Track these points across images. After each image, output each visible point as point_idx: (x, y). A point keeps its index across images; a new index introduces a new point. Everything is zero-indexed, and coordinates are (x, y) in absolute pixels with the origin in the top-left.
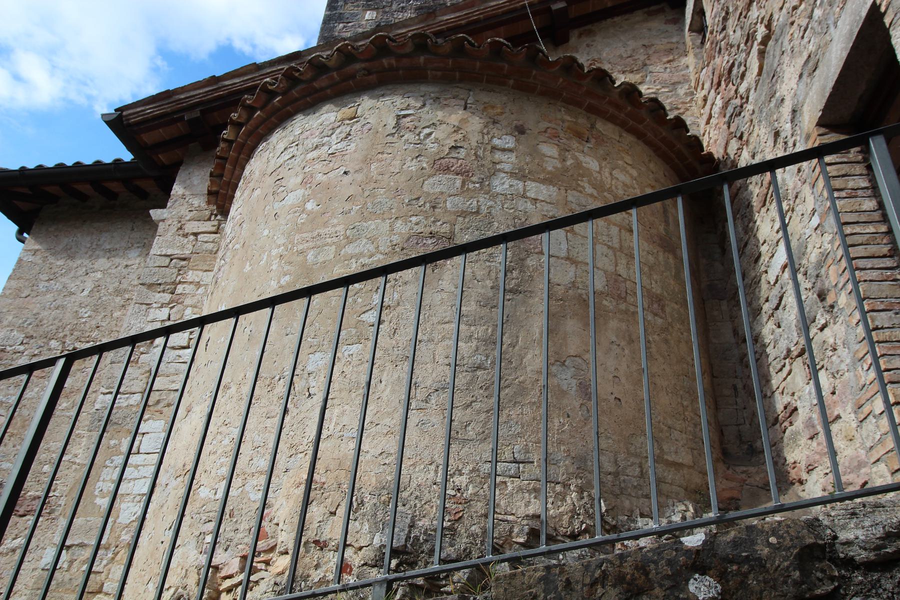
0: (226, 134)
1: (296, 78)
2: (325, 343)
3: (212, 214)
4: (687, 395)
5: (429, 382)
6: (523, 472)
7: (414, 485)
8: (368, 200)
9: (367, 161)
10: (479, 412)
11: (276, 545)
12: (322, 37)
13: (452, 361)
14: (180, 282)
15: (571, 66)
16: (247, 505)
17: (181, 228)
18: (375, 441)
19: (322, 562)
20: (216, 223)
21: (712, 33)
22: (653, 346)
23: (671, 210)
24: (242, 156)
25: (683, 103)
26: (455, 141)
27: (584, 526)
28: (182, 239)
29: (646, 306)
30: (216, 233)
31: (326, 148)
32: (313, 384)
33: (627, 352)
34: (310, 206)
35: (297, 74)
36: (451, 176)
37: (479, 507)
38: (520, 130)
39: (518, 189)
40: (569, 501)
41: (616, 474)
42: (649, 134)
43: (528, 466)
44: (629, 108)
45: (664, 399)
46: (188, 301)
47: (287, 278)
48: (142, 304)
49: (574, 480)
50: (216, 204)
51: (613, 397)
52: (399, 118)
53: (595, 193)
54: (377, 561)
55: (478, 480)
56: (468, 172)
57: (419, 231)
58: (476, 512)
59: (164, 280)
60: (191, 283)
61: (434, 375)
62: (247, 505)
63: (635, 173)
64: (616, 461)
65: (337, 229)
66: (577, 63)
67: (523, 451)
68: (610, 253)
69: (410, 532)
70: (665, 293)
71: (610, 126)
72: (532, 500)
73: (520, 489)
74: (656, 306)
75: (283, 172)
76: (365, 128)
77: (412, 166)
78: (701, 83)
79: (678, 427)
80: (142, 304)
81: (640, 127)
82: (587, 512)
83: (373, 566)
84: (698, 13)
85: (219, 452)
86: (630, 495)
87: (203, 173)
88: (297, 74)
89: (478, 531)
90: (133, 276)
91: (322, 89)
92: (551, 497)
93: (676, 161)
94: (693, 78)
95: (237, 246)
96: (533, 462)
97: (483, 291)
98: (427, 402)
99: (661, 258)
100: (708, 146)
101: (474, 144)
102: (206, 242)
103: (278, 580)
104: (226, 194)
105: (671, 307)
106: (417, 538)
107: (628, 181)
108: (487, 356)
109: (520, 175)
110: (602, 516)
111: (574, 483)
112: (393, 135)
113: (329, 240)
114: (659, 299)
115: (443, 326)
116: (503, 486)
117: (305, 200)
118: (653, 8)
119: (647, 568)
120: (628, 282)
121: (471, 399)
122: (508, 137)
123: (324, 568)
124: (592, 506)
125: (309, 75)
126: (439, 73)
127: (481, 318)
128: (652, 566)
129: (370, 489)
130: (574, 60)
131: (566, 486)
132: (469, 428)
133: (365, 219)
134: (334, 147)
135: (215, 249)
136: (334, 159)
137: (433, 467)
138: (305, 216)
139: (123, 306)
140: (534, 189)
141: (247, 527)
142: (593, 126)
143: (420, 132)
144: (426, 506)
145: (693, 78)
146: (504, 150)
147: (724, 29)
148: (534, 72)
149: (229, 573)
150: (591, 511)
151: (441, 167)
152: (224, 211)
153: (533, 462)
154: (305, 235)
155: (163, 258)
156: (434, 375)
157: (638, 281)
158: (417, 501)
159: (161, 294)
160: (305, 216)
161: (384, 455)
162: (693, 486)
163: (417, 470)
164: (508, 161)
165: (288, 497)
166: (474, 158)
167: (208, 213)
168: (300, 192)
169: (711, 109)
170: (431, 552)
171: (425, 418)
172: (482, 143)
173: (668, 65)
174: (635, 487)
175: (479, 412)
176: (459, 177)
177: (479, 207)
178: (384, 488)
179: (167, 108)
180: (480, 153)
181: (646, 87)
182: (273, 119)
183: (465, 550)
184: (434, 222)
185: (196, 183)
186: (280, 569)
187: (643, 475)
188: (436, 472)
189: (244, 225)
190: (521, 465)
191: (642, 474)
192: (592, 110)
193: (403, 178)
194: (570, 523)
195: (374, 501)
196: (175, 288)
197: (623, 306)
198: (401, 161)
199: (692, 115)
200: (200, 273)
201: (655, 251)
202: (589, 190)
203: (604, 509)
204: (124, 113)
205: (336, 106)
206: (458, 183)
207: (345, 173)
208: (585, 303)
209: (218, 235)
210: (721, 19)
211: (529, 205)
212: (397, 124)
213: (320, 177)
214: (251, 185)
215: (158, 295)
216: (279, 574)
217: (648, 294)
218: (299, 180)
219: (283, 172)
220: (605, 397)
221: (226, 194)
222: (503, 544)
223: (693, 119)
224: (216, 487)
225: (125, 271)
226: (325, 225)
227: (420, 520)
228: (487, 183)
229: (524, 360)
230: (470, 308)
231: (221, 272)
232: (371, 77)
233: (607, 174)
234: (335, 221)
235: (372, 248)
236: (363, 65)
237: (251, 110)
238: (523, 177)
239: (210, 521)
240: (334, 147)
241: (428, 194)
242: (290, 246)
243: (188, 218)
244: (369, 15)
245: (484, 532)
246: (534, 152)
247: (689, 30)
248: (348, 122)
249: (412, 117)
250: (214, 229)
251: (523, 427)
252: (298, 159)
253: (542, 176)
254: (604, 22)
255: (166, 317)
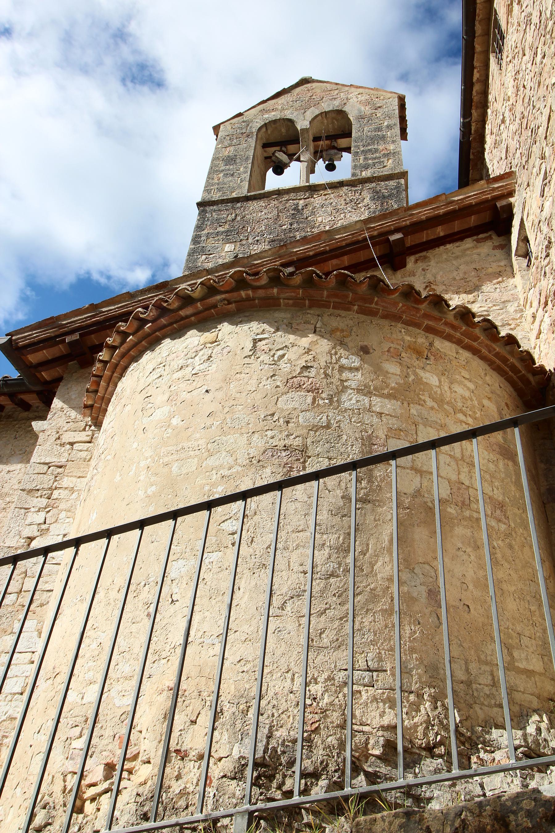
0: (103, 355)
1: (165, 307)
2: (188, 550)
3: (86, 425)
4: (534, 600)
5: (284, 590)
6: (377, 681)
7: (271, 693)
8: (228, 416)
9: (227, 380)
10: (332, 620)
11: (139, 753)
12: (188, 268)
13: (309, 568)
14: (56, 488)
15: (410, 293)
16: (112, 711)
17: (59, 438)
18: (234, 649)
19: (184, 772)
20: (90, 433)
21: (536, 259)
22: (498, 551)
23: (509, 437)
24: (115, 375)
25: (513, 319)
26: (306, 361)
27: (439, 737)
28: (59, 448)
29: (489, 513)
30: (90, 442)
31: (190, 368)
32: (175, 590)
33: (472, 557)
34: (175, 421)
35: (165, 305)
36: (302, 393)
37: (335, 717)
38: (365, 350)
39: (364, 404)
40: (423, 711)
41: (469, 683)
42: (483, 350)
43: (382, 675)
44: (464, 328)
45: (511, 605)
46: (62, 506)
47: (154, 488)
48: (21, 508)
49: (427, 689)
50: (91, 415)
51: (462, 603)
52: (255, 341)
53: (436, 406)
54: (236, 773)
55: (333, 688)
56: (318, 389)
57: (274, 444)
58: (332, 722)
59: (42, 486)
60: (66, 488)
61: (289, 582)
62: (112, 711)
63: (471, 386)
64: (467, 670)
65: (199, 443)
66: (415, 290)
67: (375, 660)
68: (453, 463)
69: (268, 743)
70: (507, 499)
71: (447, 344)
72: (387, 710)
73: (375, 699)
74: (498, 512)
75: (151, 391)
76: (226, 351)
77: (269, 385)
78: (529, 302)
79: (527, 633)
80: (21, 508)
81: (475, 344)
82: (441, 722)
83: (233, 779)
84: (523, 240)
85: (87, 656)
86: (483, 704)
87: (80, 388)
88: (165, 305)
89: (335, 742)
90: (15, 481)
91: (187, 317)
92: (405, 707)
93: (510, 373)
94: (522, 297)
95: (109, 457)
96: (386, 671)
97: (334, 501)
98: (283, 609)
99: (501, 465)
100: (539, 358)
101: (323, 364)
102: (81, 451)
103: (140, 790)
104: (100, 408)
105: (511, 511)
106: (275, 749)
107: (467, 394)
108: (340, 564)
109: (364, 390)
110: (457, 726)
111: (427, 692)
112: (250, 356)
113: (192, 453)
114: (501, 506)
115: (297, 534)
116: (358, 695)
117: (171, 416)
118: (481, 236)
119: (507, 819)
120: (471, 490)
121: (325, 606)
122: (354, 357)
123: (185, 779)
124: (446, 717)
125: (176, 305)
126: (291, 302)
127: (333, 526)
128: (512, 817)
129: (229, 697)
130: (411, 288)
131: (420, 696)
132: (323, 636)
133: (224, 433)
134: (197, 368)
135: (88, 457)
136: (197, 379)
137: (289, 675)
138: (170, 431)
139: (4, 509)
140: (379, 404)
141: (112, 734)
142: (431, 344)
143: (274, 354)
144: (283, 716)
145: (522, 297)
146: (351, 369)
147: (547, 256)
148: (376, 299)
149: (94, 781)
150: (445, 722)
151: (293, 385)
152: (98, 424)
153: (386, 671)
154: (170, 448)
155: (42, 465)
156: (289, 582)
157: (479, 487)
158: (274, 711)
159: (39, 499)
160: (170, 431)
161: (242, 663)
162: (546, 695)
163: (274, 677)
164: (355, 379)
165: (151, 704)
166: (323, 376)
167: (83, 424)
168: (166, 409)
169: (540, 326)
170: (291, 763)
171: (281, 625)
172: (331, 363)
173: (498, 286)
174: (488, 696)
175: (332, 620)
176: (310, 393)
177: (329, 422)
178: (242, 696)
179: (50, 333)
180: (329, 371)
181: (478, 305)
182: (143, 343)
183: (322, 762)
184: (287, 436)
185: (73, 397)
186: (142, 780)
187: (495, 684)
188: (293, 680)
189: (116, 438)
190: (375, 674)
191: (494, 683)
192: (429, 330)
193: (258, 396)
194: (425, 735)
195: (234, 709)
196: (52, 494)
197: (467, 513)
198: (255, 378)
199: (523, 330)
200: (74, 479)
201: (495, 459)
202: (430, 403)
203: (458, 719)
204: (14, 338)
205: (200, 331)
206: (309, 400)
207: (207, 391)
208: (431, 510)
209: (92, 444)
210: (544, 247)
211: (375, 420)
212: (254, 346)
213: (184, 395)
214: (123, 401)
215: (36, 500)
216: (141, 784)
217: (490, 499)
218: (166, 397)
219: (151, 391)
220: (454, 604)
221: (100, 408)
222: (359, 756)
223: (523, 333)
224: (83, 691)
225: (7, 476)
226: (189, 438)
227: (277, 730)
228: (335, 399)
229: (375, 568)
230: (324, 516)
231: (93, 481)
232: (230, 306)
233: (446, 388)
234: (198, 435)
235: (231, 460)
236: (223, 296)
237: (124, 335)
238: (369, 394)
239: (76, 726)
240: (197, 368)
241: (282, 410)
242: (156, 458)
243: (65, 429)
244: (229, 247)
245: (342, 745)
246: (378, 370)
247: (515, 255)
248: (210, 345)
249: (267, 341)
250: (88, 439)
251: (375, 635)
252: (165, 378)
253: (386, 392)
254: (437, 249)
255: (42, 521)
